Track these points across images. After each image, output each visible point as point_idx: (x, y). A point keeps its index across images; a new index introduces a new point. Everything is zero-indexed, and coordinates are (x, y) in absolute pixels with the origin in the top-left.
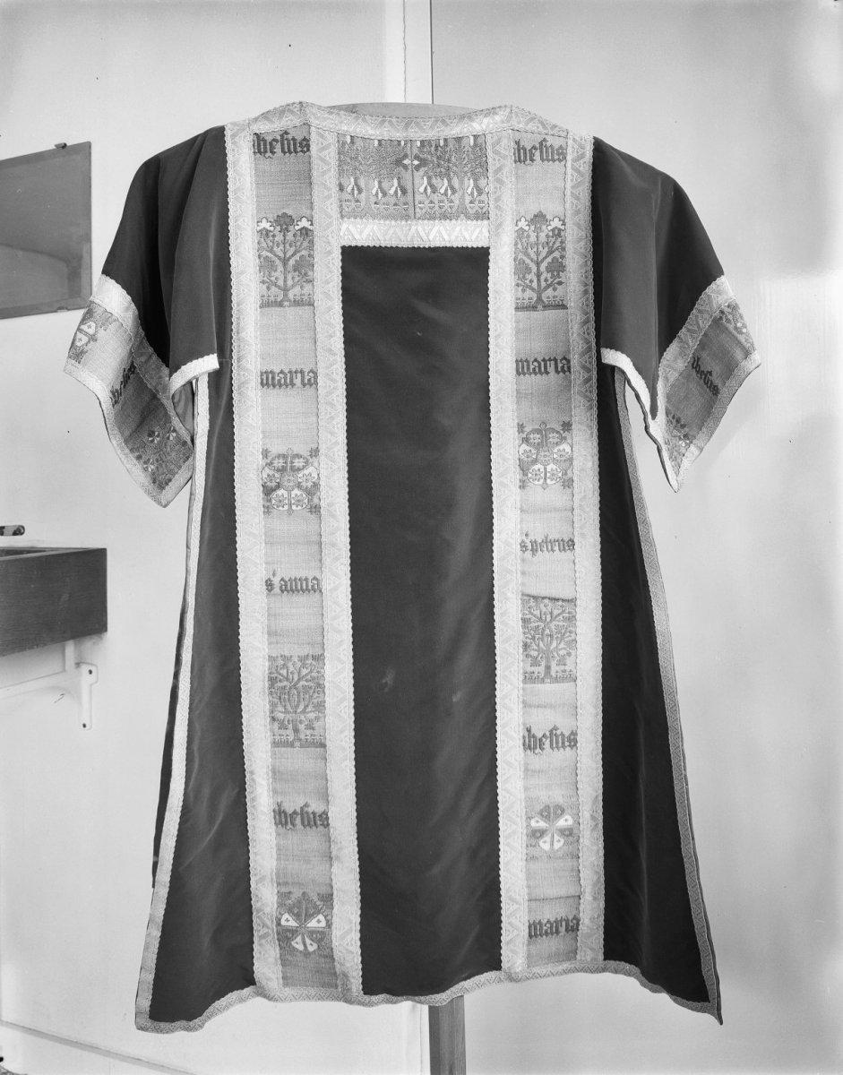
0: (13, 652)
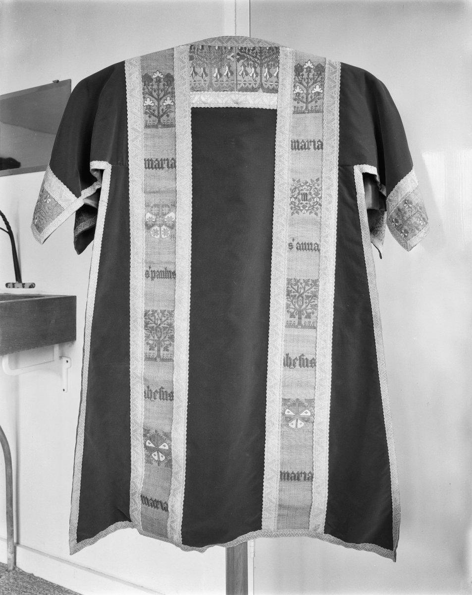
0: (24, 350)
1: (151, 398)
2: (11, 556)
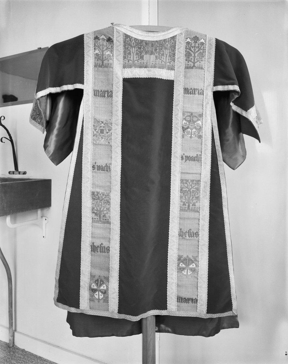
0: (20, 212)
1: (95, 251)
2: (11, 338)
